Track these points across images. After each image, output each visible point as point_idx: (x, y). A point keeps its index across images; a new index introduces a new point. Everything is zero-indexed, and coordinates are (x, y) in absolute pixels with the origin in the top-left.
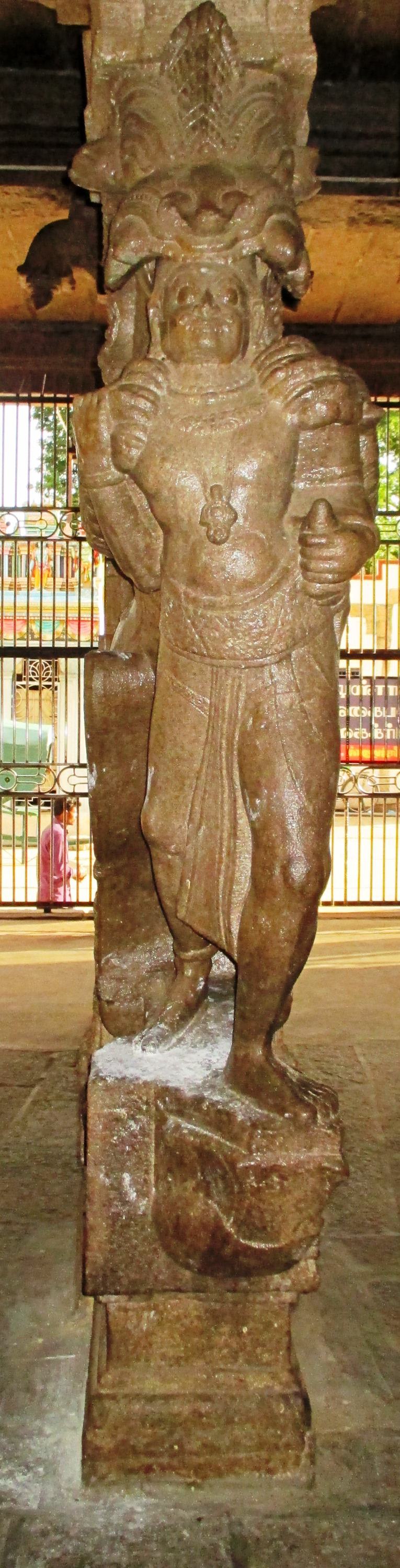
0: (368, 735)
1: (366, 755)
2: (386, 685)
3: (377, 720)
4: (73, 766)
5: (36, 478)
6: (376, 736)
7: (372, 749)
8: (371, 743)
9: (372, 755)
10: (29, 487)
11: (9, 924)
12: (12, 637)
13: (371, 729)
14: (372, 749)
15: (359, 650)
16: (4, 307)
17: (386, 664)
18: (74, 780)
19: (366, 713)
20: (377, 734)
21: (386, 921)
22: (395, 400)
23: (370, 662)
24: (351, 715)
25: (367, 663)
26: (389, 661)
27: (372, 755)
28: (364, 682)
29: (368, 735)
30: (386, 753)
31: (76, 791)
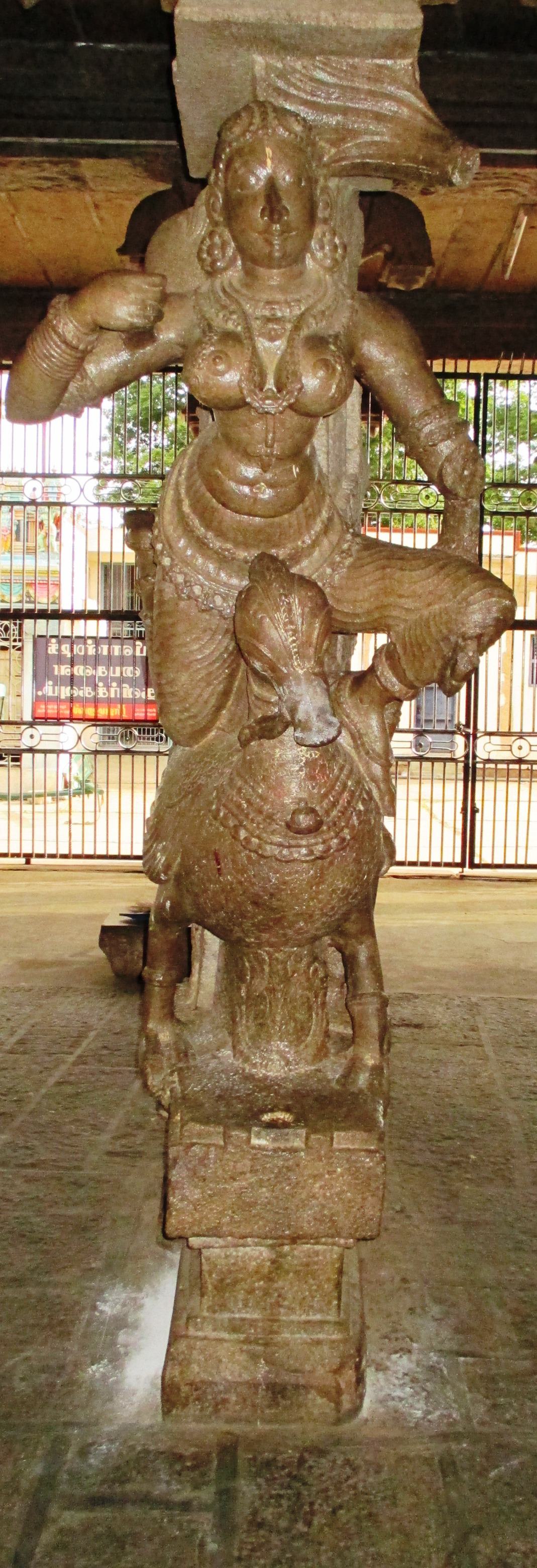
0: (93, 694)
1: (90, 712)
2: (110, 645)
3: (101, 679)
4: (491, 734)
5: (106, 446)
6: (101, 695)
7: (96, 707)
8: (96, 702)
9: (96, 713)
10: (88, 455)
11: (505, 887)
12: (45, 601)
13: (95, 687)
14: (96, 707)
15: (9, 610)
16: (6, 278)
17: (72, 624)
18: (489, 747)
19: (90, 672)
20: (102, 692)
21: (101, 874)
22: (528, 366)
23: (82, 621)
24: (76, 673)
25: (92, 623)
26: (76, 622)
27: (96, 713)
28: (90, 641)
29: (93, 694)
30: (46, 709)
31: (492, 758)
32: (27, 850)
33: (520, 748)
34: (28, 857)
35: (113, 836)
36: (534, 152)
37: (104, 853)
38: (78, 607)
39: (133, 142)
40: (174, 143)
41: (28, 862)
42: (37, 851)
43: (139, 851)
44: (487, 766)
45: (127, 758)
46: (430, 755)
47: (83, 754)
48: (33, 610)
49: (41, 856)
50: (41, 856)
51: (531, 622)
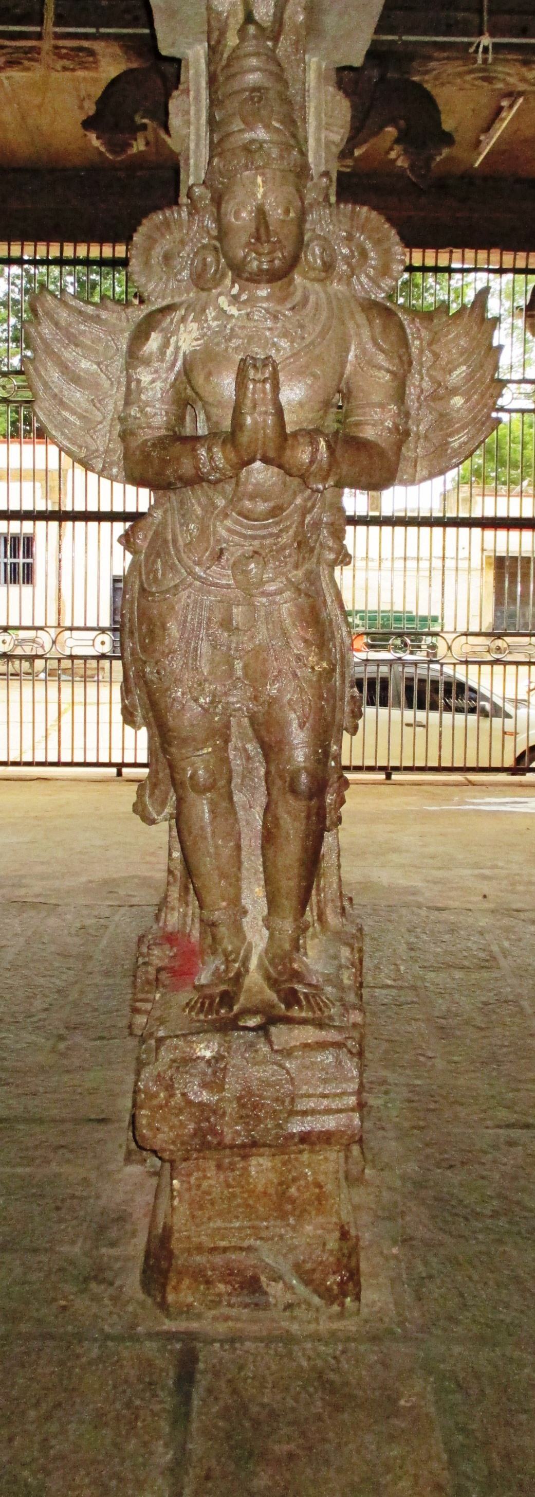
17: (60, 526)
25: (514, 534)
32: (117, 759)
33: (103, 643)
34: (120, 766)
35: (91, 743)
36: (533, 41)
37: (69, 760)
38: (27, 506)
39: (427, 39)
40: (147, 31)
41: (119, 774)
42: (129, 759)
43: (143, 758)
44: (432, 666)
45: (498, 669)
46: (509, 658)
47: (454, 664)
48: (379, 517)
49: (358, 769)
50: (358, 769)
51: (528, 519)
